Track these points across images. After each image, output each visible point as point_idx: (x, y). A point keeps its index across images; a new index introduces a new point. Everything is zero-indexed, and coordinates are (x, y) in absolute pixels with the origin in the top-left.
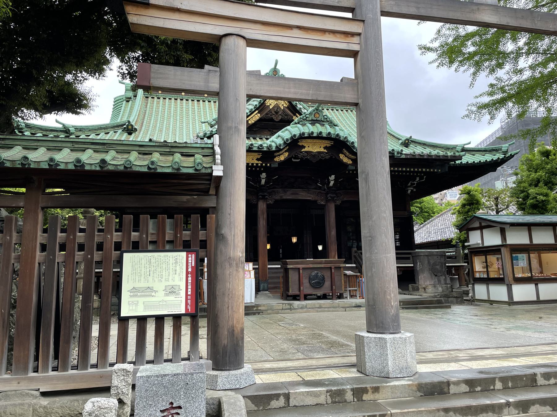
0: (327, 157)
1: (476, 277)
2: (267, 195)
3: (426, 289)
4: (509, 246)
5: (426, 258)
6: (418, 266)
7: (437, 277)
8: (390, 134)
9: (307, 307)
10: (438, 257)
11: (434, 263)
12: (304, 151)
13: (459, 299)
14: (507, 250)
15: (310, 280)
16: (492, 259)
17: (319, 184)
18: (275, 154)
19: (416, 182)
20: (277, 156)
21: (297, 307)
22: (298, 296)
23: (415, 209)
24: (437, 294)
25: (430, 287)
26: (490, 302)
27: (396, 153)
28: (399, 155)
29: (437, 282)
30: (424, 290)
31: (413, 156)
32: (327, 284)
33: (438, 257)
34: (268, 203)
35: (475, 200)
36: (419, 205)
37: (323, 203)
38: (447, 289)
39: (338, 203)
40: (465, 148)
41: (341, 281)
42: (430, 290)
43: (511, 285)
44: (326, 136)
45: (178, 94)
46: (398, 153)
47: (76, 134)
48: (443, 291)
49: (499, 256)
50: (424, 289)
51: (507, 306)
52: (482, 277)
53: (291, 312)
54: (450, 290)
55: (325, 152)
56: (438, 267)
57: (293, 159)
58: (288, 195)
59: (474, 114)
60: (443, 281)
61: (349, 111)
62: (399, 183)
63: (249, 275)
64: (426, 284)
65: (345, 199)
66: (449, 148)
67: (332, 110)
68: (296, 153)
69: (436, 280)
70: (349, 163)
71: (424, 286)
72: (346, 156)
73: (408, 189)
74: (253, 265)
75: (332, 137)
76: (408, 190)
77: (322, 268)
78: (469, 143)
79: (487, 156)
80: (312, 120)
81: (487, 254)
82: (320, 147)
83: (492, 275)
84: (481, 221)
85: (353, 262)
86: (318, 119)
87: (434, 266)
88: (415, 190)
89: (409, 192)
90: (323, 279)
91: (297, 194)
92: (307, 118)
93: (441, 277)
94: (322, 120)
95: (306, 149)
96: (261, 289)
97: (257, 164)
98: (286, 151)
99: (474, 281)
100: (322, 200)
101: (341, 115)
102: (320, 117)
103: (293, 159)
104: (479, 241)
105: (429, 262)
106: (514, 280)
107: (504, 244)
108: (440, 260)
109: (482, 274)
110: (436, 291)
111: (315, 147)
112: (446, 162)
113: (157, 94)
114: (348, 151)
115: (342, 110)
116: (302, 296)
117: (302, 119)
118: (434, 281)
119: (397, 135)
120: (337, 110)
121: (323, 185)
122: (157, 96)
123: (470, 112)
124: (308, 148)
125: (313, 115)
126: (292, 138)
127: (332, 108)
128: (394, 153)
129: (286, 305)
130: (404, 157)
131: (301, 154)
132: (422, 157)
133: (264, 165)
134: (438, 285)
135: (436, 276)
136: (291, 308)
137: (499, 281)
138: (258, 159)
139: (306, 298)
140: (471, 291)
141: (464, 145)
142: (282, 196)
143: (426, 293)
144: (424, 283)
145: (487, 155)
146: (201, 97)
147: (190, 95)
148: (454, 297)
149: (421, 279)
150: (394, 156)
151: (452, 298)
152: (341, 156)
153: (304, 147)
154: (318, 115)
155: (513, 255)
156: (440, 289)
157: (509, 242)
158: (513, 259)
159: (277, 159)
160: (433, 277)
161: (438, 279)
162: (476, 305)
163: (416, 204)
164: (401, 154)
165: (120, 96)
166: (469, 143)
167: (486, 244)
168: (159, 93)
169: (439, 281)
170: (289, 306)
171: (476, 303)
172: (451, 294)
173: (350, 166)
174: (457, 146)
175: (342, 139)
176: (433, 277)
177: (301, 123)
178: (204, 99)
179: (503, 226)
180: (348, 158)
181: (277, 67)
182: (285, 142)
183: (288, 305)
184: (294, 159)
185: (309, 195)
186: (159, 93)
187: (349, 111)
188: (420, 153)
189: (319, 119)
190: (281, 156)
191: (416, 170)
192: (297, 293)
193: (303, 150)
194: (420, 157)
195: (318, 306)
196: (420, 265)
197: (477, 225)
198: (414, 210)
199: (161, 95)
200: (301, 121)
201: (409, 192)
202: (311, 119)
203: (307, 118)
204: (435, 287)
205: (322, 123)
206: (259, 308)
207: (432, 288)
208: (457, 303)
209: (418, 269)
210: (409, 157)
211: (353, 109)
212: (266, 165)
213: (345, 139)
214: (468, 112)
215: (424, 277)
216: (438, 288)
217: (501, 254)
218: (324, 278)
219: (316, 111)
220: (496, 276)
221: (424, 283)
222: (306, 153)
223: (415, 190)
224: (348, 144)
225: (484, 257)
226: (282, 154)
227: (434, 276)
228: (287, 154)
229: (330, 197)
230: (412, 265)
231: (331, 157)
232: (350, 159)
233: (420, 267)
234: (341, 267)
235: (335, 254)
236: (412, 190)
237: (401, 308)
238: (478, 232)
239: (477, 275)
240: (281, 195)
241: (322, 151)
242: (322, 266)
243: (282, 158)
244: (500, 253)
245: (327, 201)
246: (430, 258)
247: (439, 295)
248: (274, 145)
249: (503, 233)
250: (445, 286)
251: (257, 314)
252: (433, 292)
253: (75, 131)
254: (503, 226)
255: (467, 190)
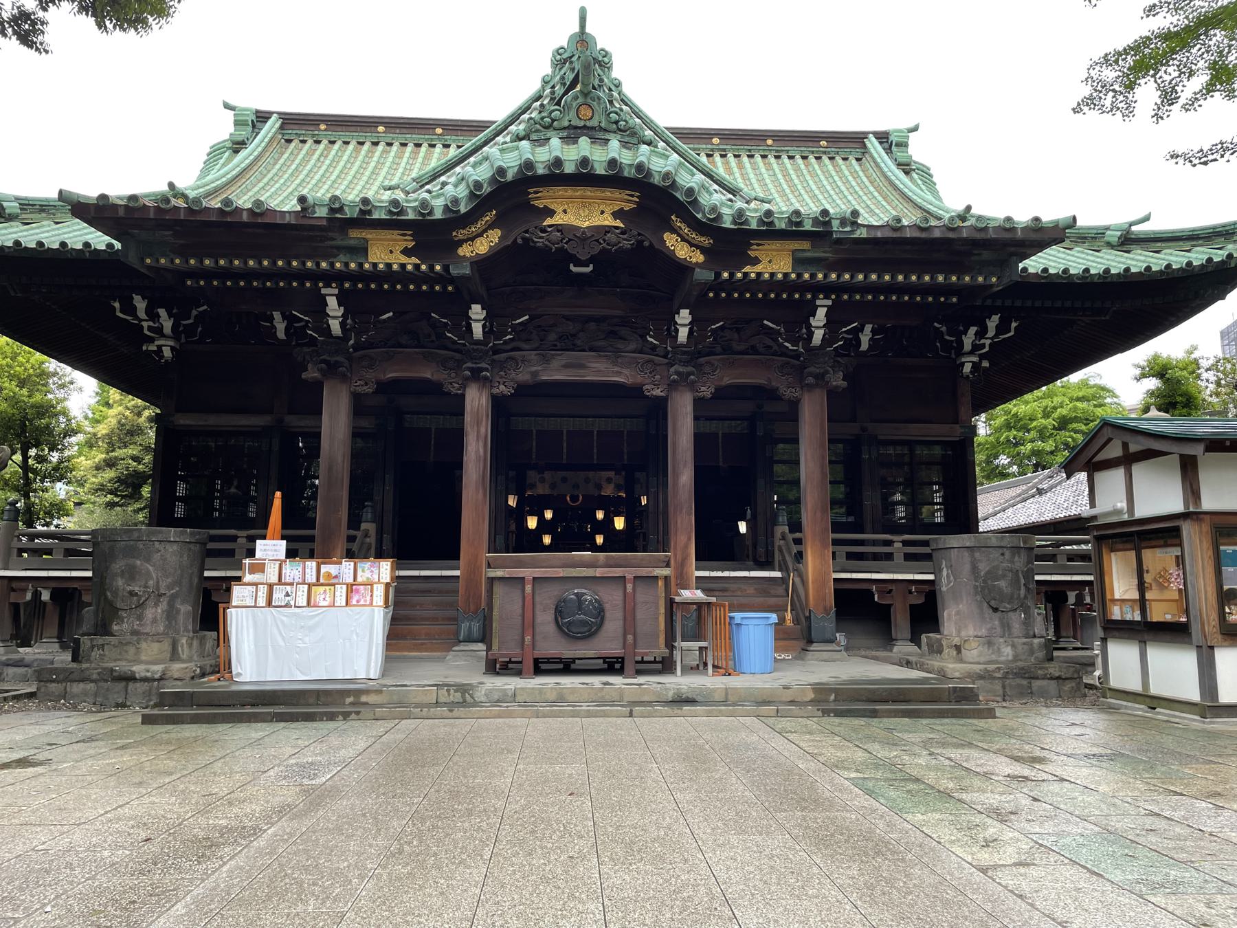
0: (627, 245)
1: (1114, 618)
2: (487, 370)
3: (963, 650)
4: (1208, 517)
5: (966, 554)
6: (944, 581)
7: (999, 614)
8: (920, 208)
9: (519, 698)
10: (1003, 554)
11: (988, 572)
12: (550, 226)
13: (1068, 686)
14: (1201, 532)
15: (559, 612)
16: (1158, 559)
17: (650, 339)
18: (454, 234)
19: (988, 342)
20: (466, 241)
21: (483, 699)
22: (621, 660)
23: (1072, 437)
24: (992, 667)
25: (974, 645)
26: (1148, 700)
27: (835, 225)
28: (848, 229)
29: (999, 630)
30: (955, 653)
31: (895, 230)
32: (613, 624)
33: (1003, 554)
34: (495, 391)
35: (1181, 395)
36: (1084, 427)
37: (658, 392)
38: (1032, 652)
39: (706, 391)
40: (1133, 233)
41: (657, 618)
42: (974, 652)
43: (1212, 648)
44: (603, 172)
45: (368, 129)
46: (843, 222)
47: (24, 219)
48: (1016, 658)
49: (1176, 551)
50: (958, 648)
51: (1197, 718)
52: (1128, 617)
53: (450, 714)
54: (1041, 654)
55: (617, 228)
56: (1002, 584)
57: (571, 265)
58: (556, 371)
59: (1111, 94)
60: (1017, 628)
61: (825, 158)
62: (938, 344)
63: (368, 598)
64: (963, 633)
65: (727, 381)
66: (1085, 238)
67: (778, 157)
68: (527, 232)
69: (997, 623)
70: (694, 260)
71: (956, 641)
72: (683, 239)
73: (963, 360)
74: (393, 570)
75: (626, 174)
76: (962, 364)
77: (595, 578)
78: (1147, 219)
79: (1197, 252)
80: (570, 127)
81: (1143, 545)
82: (602, 212)
83: (1159, 613)
84: (1128, 438)
85: (777, 567)
86: (589, 124)
87: (989, 582)
88: (985, 364)
89: (967, 368)
90: (600, 613)
91: (582, 366)
92: (553, 121)
93: (1011, 614)
94: (603, 125)
95: (558, 219)
96: (461, 638)
97: (403, 266)
98: (491, 226)
99: (1105, 629)
100: (657, 385)
101: (797, 170)
102: (596, 117)
103: (571, 265)
104: (1121, 502)
105: (974, 568)
106: (1221, 633)
107: (1191, 509)
108: (1012, 562)
109: (1128, 609)
110: (994, 657)
111: (587, 211)
112: (1013, 249)
113: (316, 132)
114: (684, 221)
115: (804, 158)
116: (529, 664)
117: (538, 126)
118: (989, 626)
119: (935, 209)
120: (791, 158)
121: (662, 341)
122: (313, 136)
123: (1099, 88)
124: (562, 215)
125: (573, 113)
126: (493, 180)
127: (777, 151)
128: (828, 223)
129: (448, 691)
130: (864, 235)
131: (544, 235)
132: (924, 235)
133: (424, 267)
134: (1001, 640)
135: (995, 610)
136: (465, 701)
137: (1174, 632)
138: (406, 252)
139: (541, 669)
140: (1099, 661)
141: (1131, 225)
142: (535, 374)
143: (961, 661)
144: (959, 631)
145: (1199, 249)
146: (427, 137)
147: (398, 131)
148: (1051, 679)
149: (949, 619)
150: (831, 233)
151: (1043, 679)
152: (670, 240)
153: (551, 213)
154: (589, 113)
155: (1222, 548)
156: (1008, 652)
157: (1209, 503)
158: (1223, 560)
159: (465, 251)
160: (987, 616)
161: (1001, 620)
162: (1111, 709)
163: (1074, 425)
164: (855, 224)
165: (219, 143)
166: (1147, 219)
167: (1142, 511)
168: (319, 130)
169: (1006, 626)
170: (459, 695)
171: (1109, 700)
172: (1040, 668)
173: (697, 270)
174: (1108, 228)
175: (656, 180)
176: (987, 616)
177: (534, 137)
178: (432, 140)
179: (1190, 450)
180: (692, 245)
181: (588, 30)
182: (471, 192)
183: (456, 691)
184: (575, 266)
185: (616, 369)
186: (319, 130)
187: (825, 158)
188: (918, 222)
189: (594, 123)
190: (478, 241)
191: (914, 278)
192: (514, 652)
193: (549, 221)
194: (917, 234)
195: (552, 696)
196: (948, 576)
197: (1114, 451)
198: (1070, 440)
199: (325, 133)
200: (537, 131)
201: (967, 368)
202: (566, 124)
203: (553, 121)
204: (990, 644)
205: (601, 135)
206: (364, 699)
207: (980, 648)
208: (1060, 697)
209: (944, 589)
210: (879, 235)
211: (838, 153)
212: (432, 268)
213: (664, 180)
214: (1089, 87)
215: (958, 613)
216: (999, 649)
217: (1180, 545)
218: (603, 611)
219: (580, 100)
220: (1168, 618)
221: (959, 631)
222: (558, 231)
223: (985, 364)
224: (678, 195)
225: (1133, 554)
226: (480, 235)
227: (991, 611)
228: (495, 236)
229: (677, 373)
230: (931, 577)
231: (640, 243)
232: (697, 247)
233: (949, 582)
234: (656, 578)
235: (689, 539)
236: (975, 366)
237: (820, 713)
238: (1118, 475)
239: (1116, 613)
240: (534, 369)
241: (607, 223)
242: (598, 572)
243: (482, 247)
244: (1176, 541)
245: (673, 386)
246: (977, 555)
247: (999, 669)
248: (438, 203)
249: (1189, 468)
250: (1024, 644)
251: (341, 717)
252: (982, 659)
253: (19, 211)
254: (1190, 450)
255: (1158, 364)
